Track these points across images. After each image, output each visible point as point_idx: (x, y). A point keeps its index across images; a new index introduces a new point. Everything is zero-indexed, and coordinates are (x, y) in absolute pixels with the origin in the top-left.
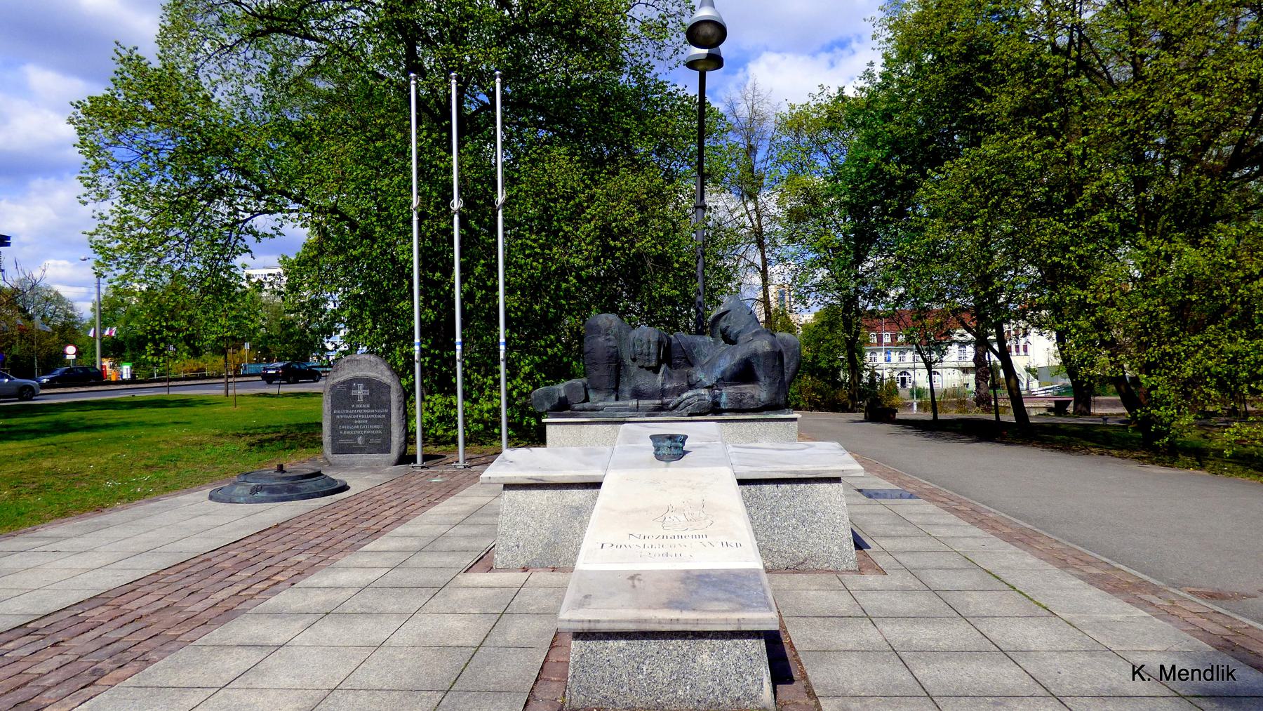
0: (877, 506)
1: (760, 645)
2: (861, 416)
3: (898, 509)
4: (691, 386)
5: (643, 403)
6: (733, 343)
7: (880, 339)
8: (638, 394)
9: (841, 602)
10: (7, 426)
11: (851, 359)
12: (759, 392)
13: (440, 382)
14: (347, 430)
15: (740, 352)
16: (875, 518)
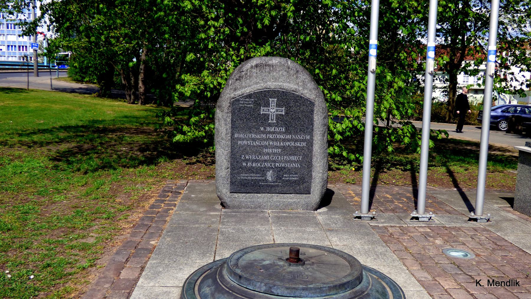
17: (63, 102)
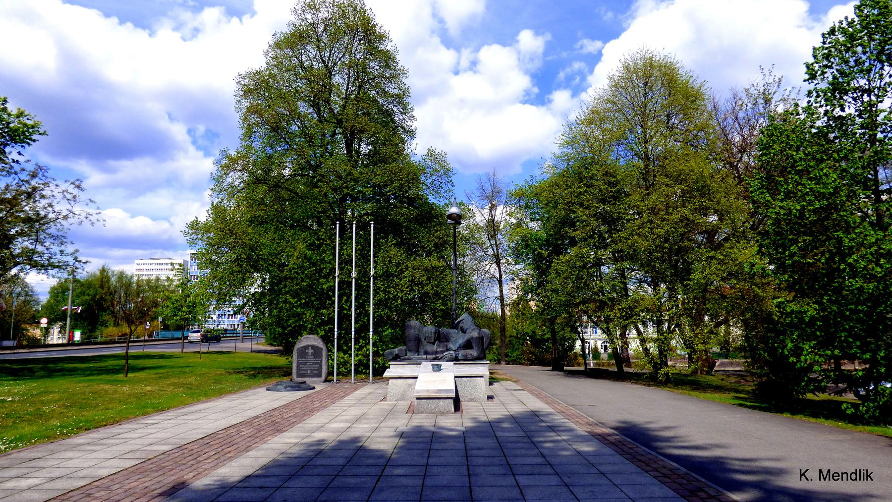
1: (451, 401)
2: (550, 368)
4: (447, 350)
8: (426, 353)
12: (474, 353)
13: (344, 348)
14: (303, 367)
15: (467, 337)
17: (257, 358)
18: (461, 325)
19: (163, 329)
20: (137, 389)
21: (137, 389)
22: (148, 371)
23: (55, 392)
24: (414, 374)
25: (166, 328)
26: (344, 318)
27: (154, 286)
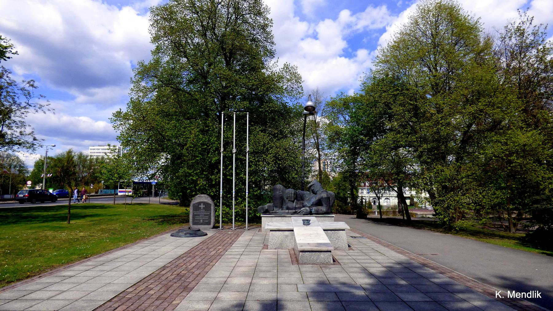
0: (355, 240)
2: (355, 216)
3: (361, 241)
4: (304, 207)
5: (290, 211)
6: (316, 194)
7: (365, 184)
8: (288, 208)
9: (345, 254)
10: (56, 215)
11: (352, 194)
12: (323, 209)
14: (197, 218)
16: (353, 242)
18: (312, 188)
19: (106, 188)
20: (73, 235)
21: (73, 235)
22: (89, 219)
23: (5, 239)
24: (290, 228)
25: (107, 187)
26: (228, 182)
27: (101, 162)
